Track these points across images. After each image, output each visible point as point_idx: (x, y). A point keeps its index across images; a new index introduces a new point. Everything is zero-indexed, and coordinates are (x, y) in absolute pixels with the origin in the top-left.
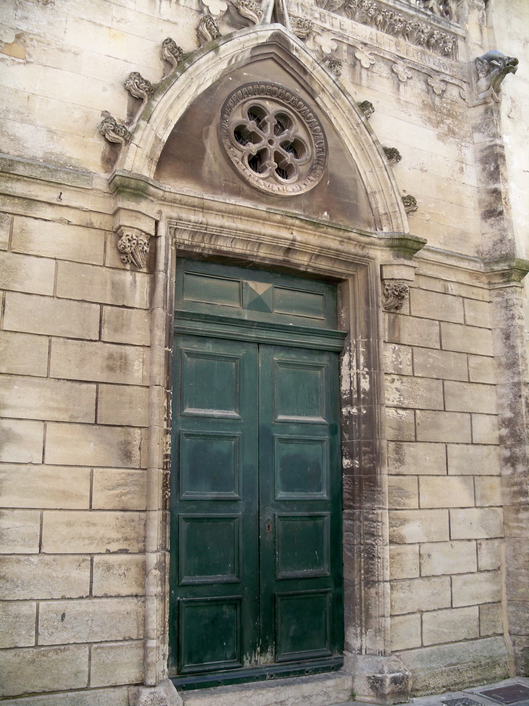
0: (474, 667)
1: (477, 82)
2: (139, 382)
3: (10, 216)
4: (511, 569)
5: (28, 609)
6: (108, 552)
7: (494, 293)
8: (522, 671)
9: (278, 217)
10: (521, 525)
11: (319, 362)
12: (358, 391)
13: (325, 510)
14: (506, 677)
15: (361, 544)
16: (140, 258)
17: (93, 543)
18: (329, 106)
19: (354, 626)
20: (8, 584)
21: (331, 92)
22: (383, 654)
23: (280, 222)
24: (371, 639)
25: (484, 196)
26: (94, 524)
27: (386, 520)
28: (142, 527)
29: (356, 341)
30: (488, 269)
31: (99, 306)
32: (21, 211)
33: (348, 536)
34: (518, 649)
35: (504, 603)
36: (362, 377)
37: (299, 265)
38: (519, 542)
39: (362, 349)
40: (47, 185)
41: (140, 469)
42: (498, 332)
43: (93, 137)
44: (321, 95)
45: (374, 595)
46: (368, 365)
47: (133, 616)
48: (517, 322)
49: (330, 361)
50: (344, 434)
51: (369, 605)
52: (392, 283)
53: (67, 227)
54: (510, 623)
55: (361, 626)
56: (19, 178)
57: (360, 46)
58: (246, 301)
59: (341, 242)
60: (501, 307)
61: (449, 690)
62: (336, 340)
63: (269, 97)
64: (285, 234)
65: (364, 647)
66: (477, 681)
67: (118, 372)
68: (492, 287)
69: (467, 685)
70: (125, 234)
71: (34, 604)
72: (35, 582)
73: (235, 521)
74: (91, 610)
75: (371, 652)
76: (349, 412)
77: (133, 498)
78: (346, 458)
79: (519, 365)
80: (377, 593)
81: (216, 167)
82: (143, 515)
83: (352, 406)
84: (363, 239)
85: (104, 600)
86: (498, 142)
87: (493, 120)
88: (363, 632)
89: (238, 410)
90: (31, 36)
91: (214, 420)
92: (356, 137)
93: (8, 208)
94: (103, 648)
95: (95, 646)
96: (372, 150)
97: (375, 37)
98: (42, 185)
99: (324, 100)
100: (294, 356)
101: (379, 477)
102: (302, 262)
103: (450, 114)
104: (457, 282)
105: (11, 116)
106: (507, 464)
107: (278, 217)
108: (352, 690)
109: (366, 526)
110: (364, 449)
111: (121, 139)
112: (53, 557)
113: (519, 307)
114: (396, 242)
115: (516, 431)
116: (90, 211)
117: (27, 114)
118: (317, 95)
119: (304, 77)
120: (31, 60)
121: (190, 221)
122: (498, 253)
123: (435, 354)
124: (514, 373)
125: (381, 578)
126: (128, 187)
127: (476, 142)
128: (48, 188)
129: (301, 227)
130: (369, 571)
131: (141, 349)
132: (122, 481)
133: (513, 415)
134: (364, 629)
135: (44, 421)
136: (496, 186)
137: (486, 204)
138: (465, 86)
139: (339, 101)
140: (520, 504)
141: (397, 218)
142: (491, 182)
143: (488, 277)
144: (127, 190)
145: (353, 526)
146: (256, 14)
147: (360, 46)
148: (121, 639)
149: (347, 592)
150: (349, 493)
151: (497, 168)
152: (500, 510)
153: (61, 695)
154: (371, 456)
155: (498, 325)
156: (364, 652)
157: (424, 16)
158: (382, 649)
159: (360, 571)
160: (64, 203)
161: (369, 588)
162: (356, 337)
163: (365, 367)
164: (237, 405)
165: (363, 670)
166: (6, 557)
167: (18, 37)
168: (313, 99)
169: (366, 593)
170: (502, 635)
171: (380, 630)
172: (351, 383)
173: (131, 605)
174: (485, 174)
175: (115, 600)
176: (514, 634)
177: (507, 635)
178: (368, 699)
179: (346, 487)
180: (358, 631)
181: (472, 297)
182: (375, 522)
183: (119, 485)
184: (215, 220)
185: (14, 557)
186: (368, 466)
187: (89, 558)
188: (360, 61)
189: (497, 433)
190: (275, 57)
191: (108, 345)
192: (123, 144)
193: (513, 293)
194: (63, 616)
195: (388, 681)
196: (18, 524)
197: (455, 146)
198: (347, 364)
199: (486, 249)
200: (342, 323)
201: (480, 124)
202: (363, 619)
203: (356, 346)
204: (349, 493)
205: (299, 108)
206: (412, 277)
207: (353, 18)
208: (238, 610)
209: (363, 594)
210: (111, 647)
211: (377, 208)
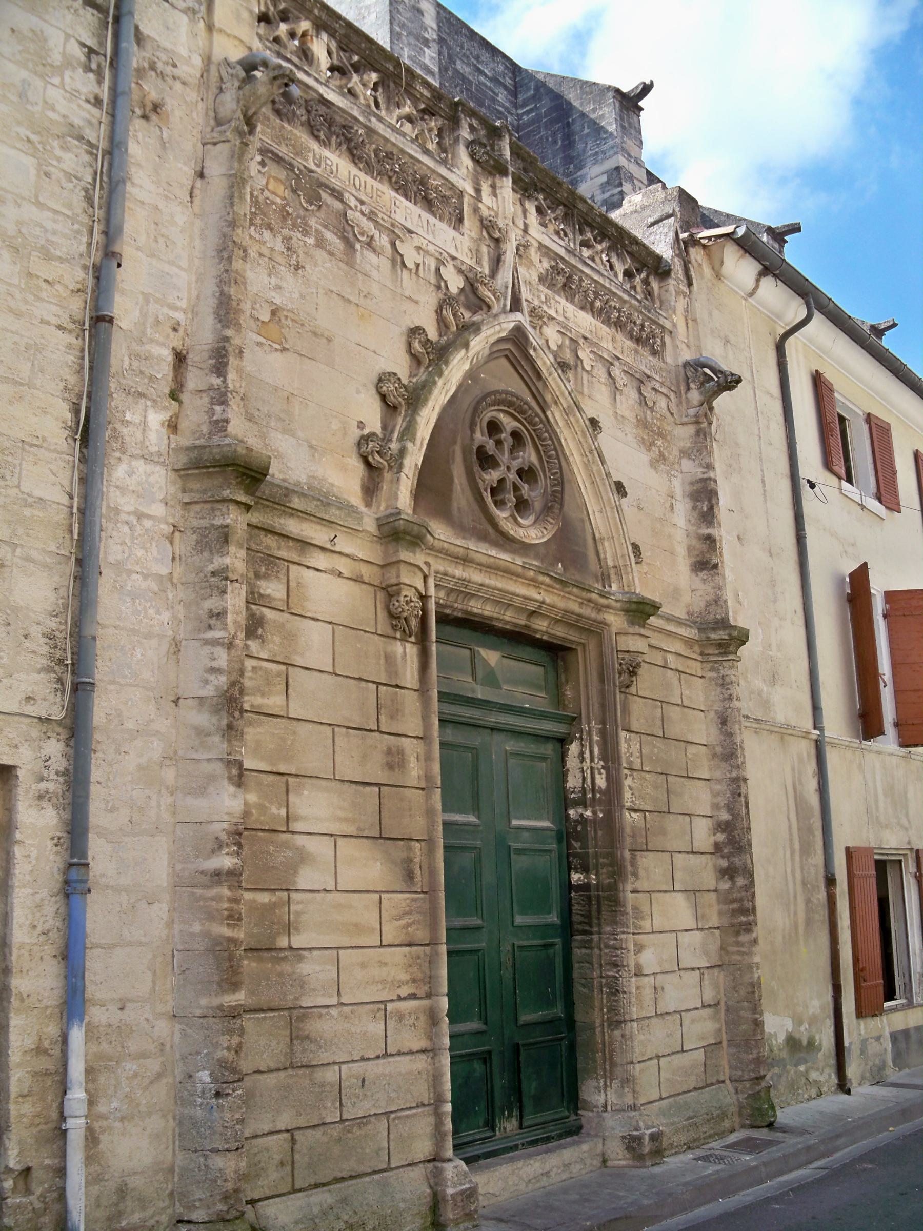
0: (708, 1120)
1: (686, 393)
2: (415, 783)
3: (286, 564)
4: (730, 1003)
5: (330, 1075)
6: (400, 998)
7: (709, 666)
8: (747, 1122)
9: (531, 574)
10: (742, 949)
11: (544, 752)
12: (593, 790)
13: (556, 937)
14: (733, 1131)
15: (601, 977)
16: (414, 623)
17: (384, 989)
18: (561, 423)
19: (596, 1078)
20: (312, 1045)
21: (565, 406)
22: (633, 1108)
23: (532, 580)
24: (616, 1092)
25: (694, 542)
26: (386, 964)
27: (631, 947)
28: (427, 964)
29: (589, 728)
30: (704, 636)
31: (375, 686)
32: (296, 558)
33: (581, 968)
34: (742, 1097)
35: (725, 1044)
36: (596, 772)
37: (536, 631)
38: (739, 969)
39: (596, 738)
40: (319, 523)
41: (423, 892)
42: (712, 715)
43: (351, 458)
44: (553, 408)
45: (619, 1038)
46: (604, 757)
47: (424, 1076)
48: (736, 703)
49: (554, 750)
50: (573, 842)
51: (613, 1050)
52: (626, 656)
53: (339, 580)
54: (730, 1067)
55: (605, 1077)
56: (294, 513)
57: (581, 341)
58: (480, 673)
59: (581, 603)
60: (716, 684)
61: (689, 1148)
62: (563, 725)
63: (506, 408)
64: (533, 593)
65: (609, 1103)
66: (710, 1136)
67: (397, 770)
68: (706, 658)
69: (702, 1141)
70: (404, 593)
71: (337, 1068)
72: (336, 1040)
73: (480, 954)
74: (387, 1072)
75: (618, 1107)
76: (581, 815)
77: (418, 930)
78: (577, 872)
79: (737, 757)
80: (623, 1036)
81: (463, 503)
82: (428, 949)
83: (585, 807)
84: (603, 601)
85: (398, 1058)
86: (712, 475)
87: (706, 446)
88: (608, 1084)
89: (476, 813)
90: (285, 313)
91: (457, 827)
92: (587, 465)
93: (283, 554)
94: (399, 1118)
95: (393, 1116)
96: (604, 484)
97: (594, 330)
98: (315, 522)
99: (556, 415)
100: (522, 745)
101: (621, 894)
102: (541, 628)
103: (661, 435)
104: (676, 653)
105: (273, 424)
106: (723, 876)
107: (531, 574)
108: (603, 1154)
109: (606, 954)
110: (601, 860)
111: (385, 463)
112: (350, 1008)
113: (736, 686)
114: (634, 606)
115: (734, 836)
116: (362, 560)
117: (287, 422)
118: (549, 407)
119: (537, 384)
120: (287, 346)
121: (454, 577)
122: (712, 616)
123: (658, 742)
124: (732, 766)
125: (627, 1017)
126: (408, 534)
127: (685, 470)
128: (318, 527)
129: (548, 586)
130: (613, 1010)
131: (415, 741)
132: (407, 909)
133: (730, 817)
134: (608, 1081)
135: (332, 835)
136: (709, 531)
137: (696, 553)
138: (672, 396)
139: (572, 419)
140: (741, 924)
141: (628, 574)
142: (703, 525)
143: (701, 646)
144: (408, 537)
145: (590, 955)
146: (494, 296)
147: (581, 341)
148: (414, 1105)
149: (581, 1038)
150: (582, 915)
151: (711, 508)
152: (717, 932)
153: (367, 1179)
154: (610, 869)
155: (711, 706)
156: (609, 1108)
157: (636, 303)
158: (631, 1103)
159: (602, 1010)
160: (337, 549)
161: (612, 1030)
162: (589, 723)
163: (600, 759)
164: (476, 809)
165: (613, 1129)
166: (310, 1011)
167: (273, 313)
168: (544, 412)
169: (610, 1037)
170: (723, 1082)
171: (628, 1080)
172: (584, 779)
173: (421, 1063)
174: (695, 514)
175: (408, 1057)
176: (736, 1081)
177: (728, 1082)
178: (623, 1163)
179: (576, 908)
180: (602, 1084)
181: (688, 671)
182: (617, 949)
183: (406, 913)
184: (477, 577)
185: (315, 1010)
186: (608, 881)
187: (382, 1007)
188: (582, 361)
189: (712, 839)
190: (510, 355)
191: (386, 736)
192: (386, 470)
193: (731, 667)
194: (363, 1081)
195: (647, 1138)
196: (318, 968)
197: (665, 475)
198: (576, 754)
199: (697, 610)
200: (566, 702)
201: (689, 448)
202: (607, 1067)
203: (589, 733)
204: (582, 915)
205: (534, 425)
206: (645, 649)
207: (572, 302)
208: (488, 1065)
209: (606, 1038)
210: (407, 1116)
211: (606, 558)
